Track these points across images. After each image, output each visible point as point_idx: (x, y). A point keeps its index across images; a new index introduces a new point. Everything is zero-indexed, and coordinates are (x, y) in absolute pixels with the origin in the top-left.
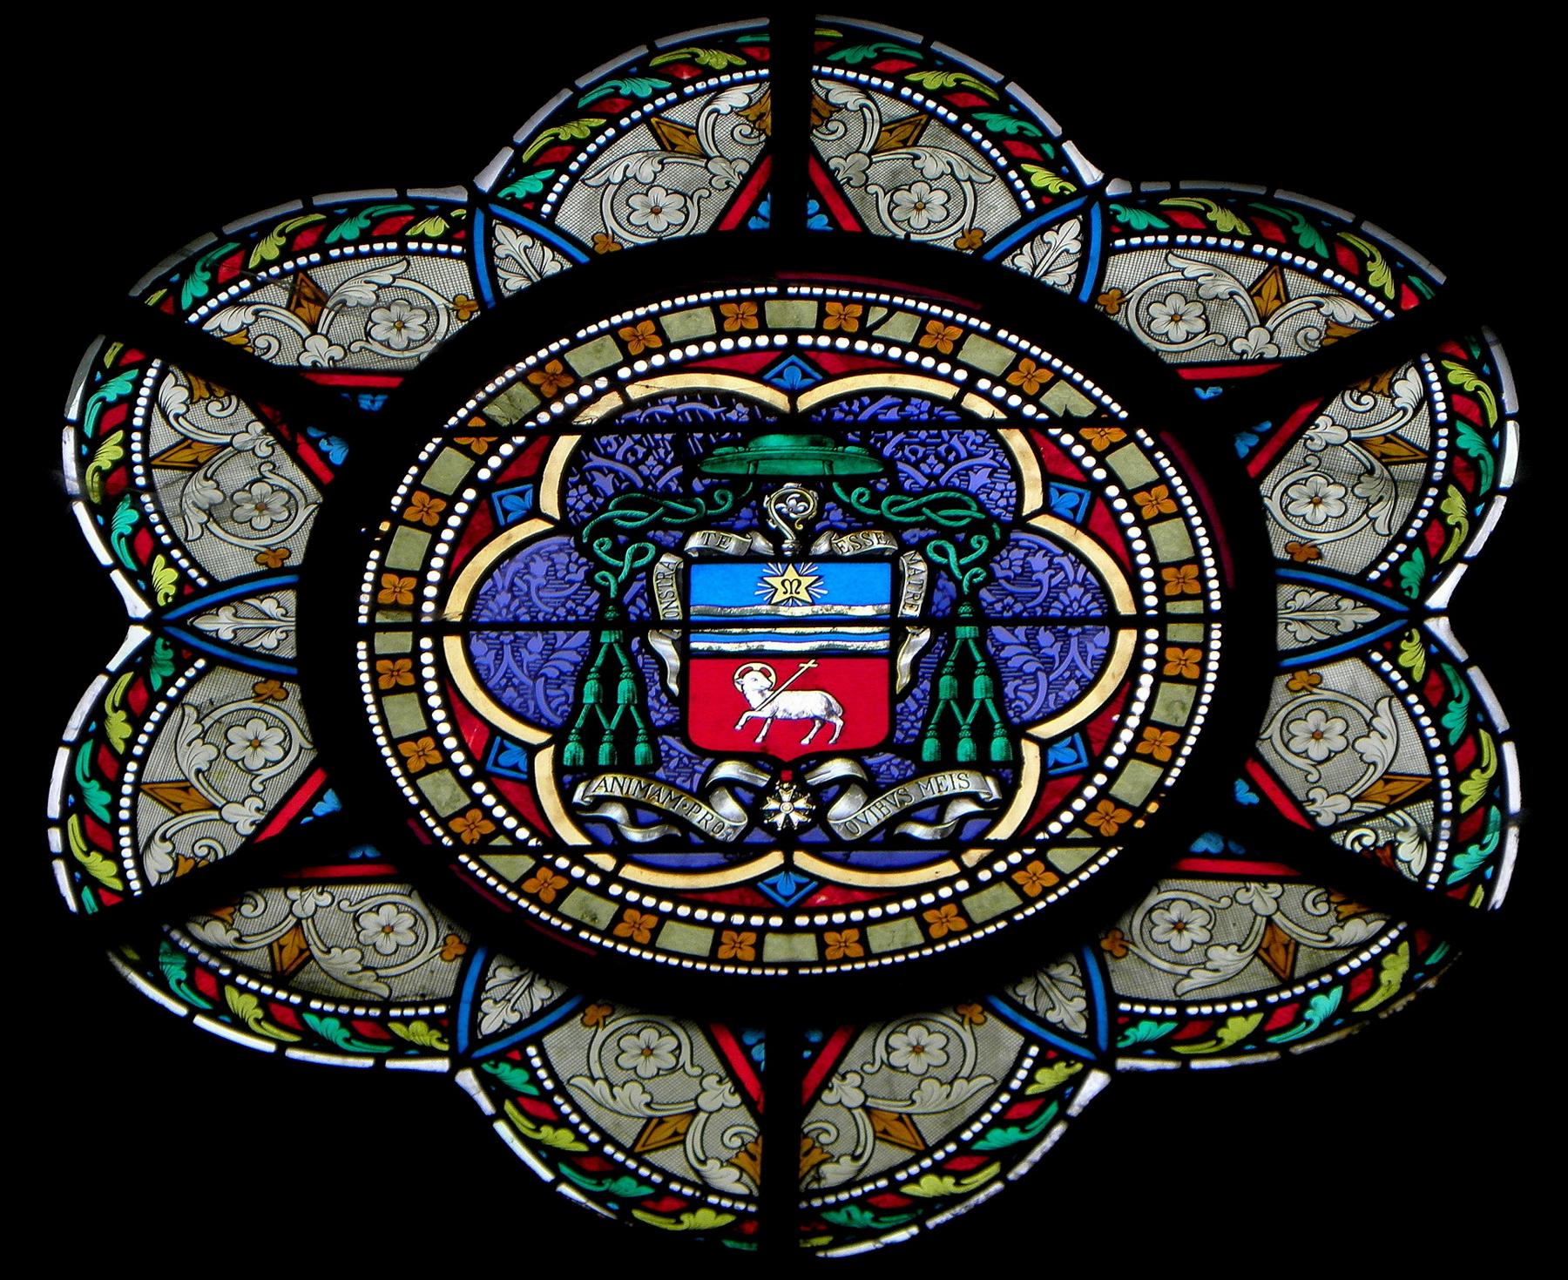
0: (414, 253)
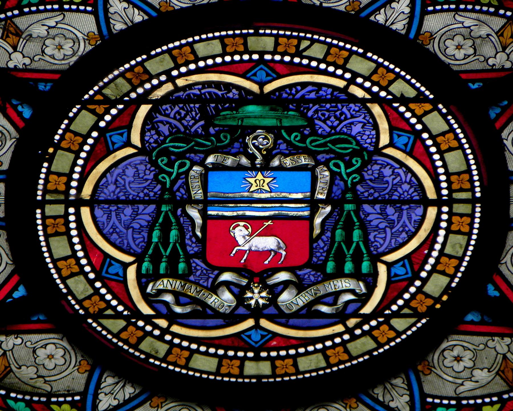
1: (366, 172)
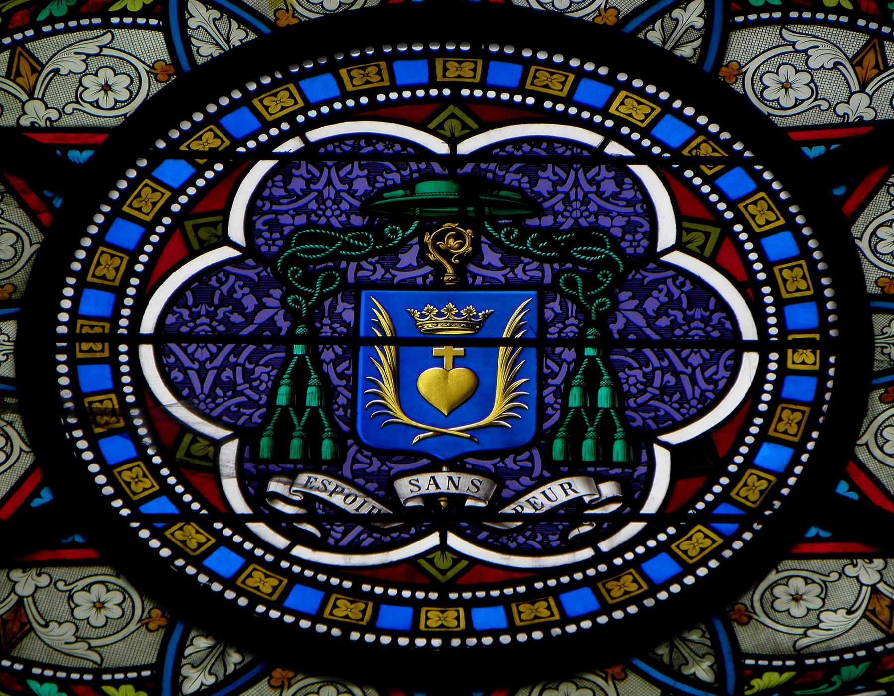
0: (116, 26)
1: (638, 381)
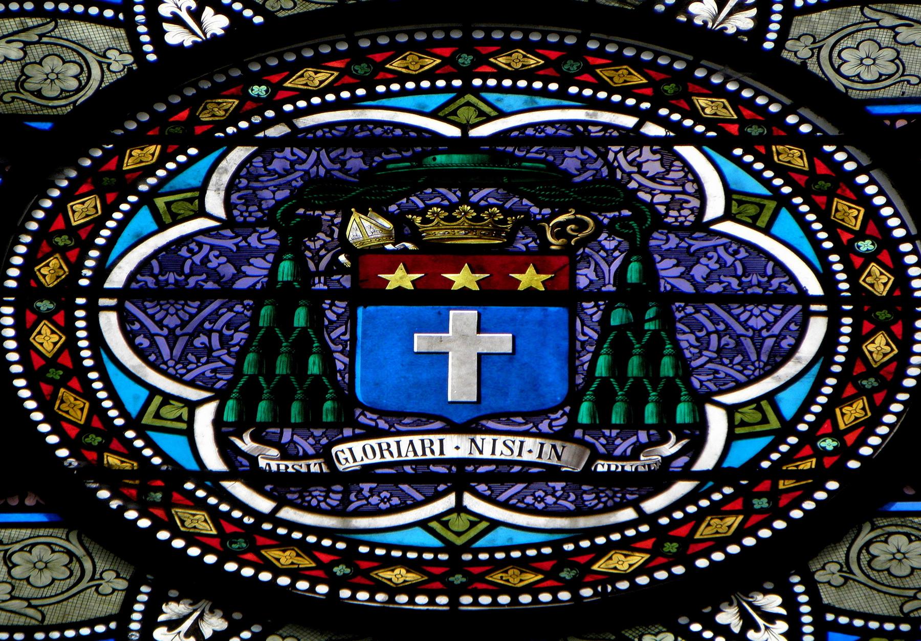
1: (691, 346)
